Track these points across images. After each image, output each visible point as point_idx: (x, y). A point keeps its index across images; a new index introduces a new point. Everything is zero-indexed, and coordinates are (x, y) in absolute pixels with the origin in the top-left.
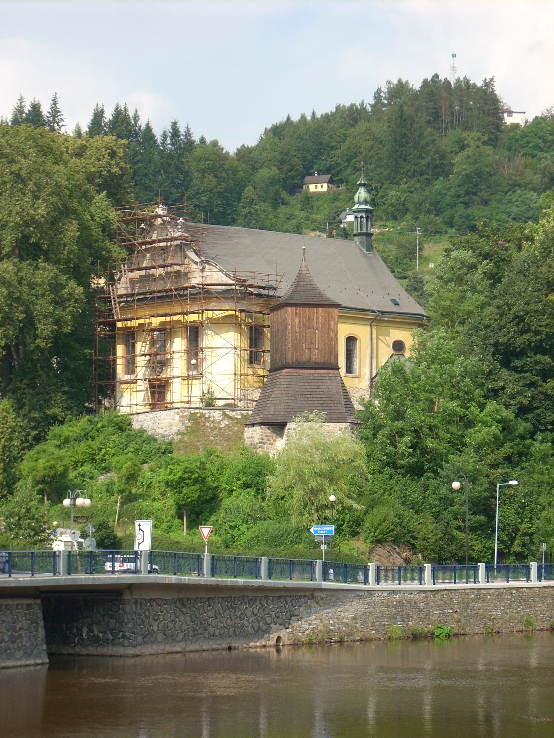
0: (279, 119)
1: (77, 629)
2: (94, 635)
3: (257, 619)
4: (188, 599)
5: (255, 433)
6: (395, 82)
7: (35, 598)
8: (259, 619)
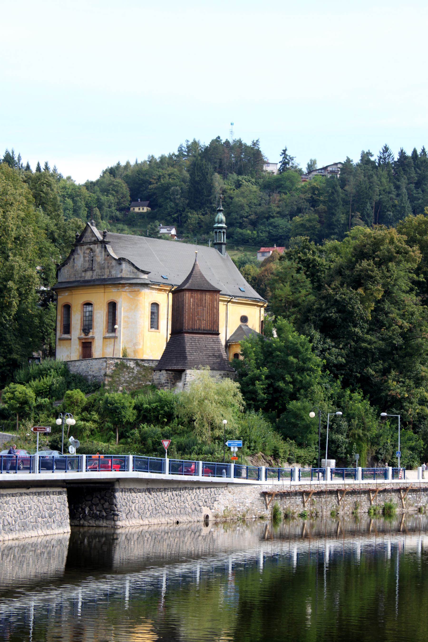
0: (112, 164)
1: (82, 509)
2: (93, 513)
3: (193, 503)
4: (153, 489)
5: (162, 376)
6: (191, 141)
7: (63, 487)
8: (195, 503)
